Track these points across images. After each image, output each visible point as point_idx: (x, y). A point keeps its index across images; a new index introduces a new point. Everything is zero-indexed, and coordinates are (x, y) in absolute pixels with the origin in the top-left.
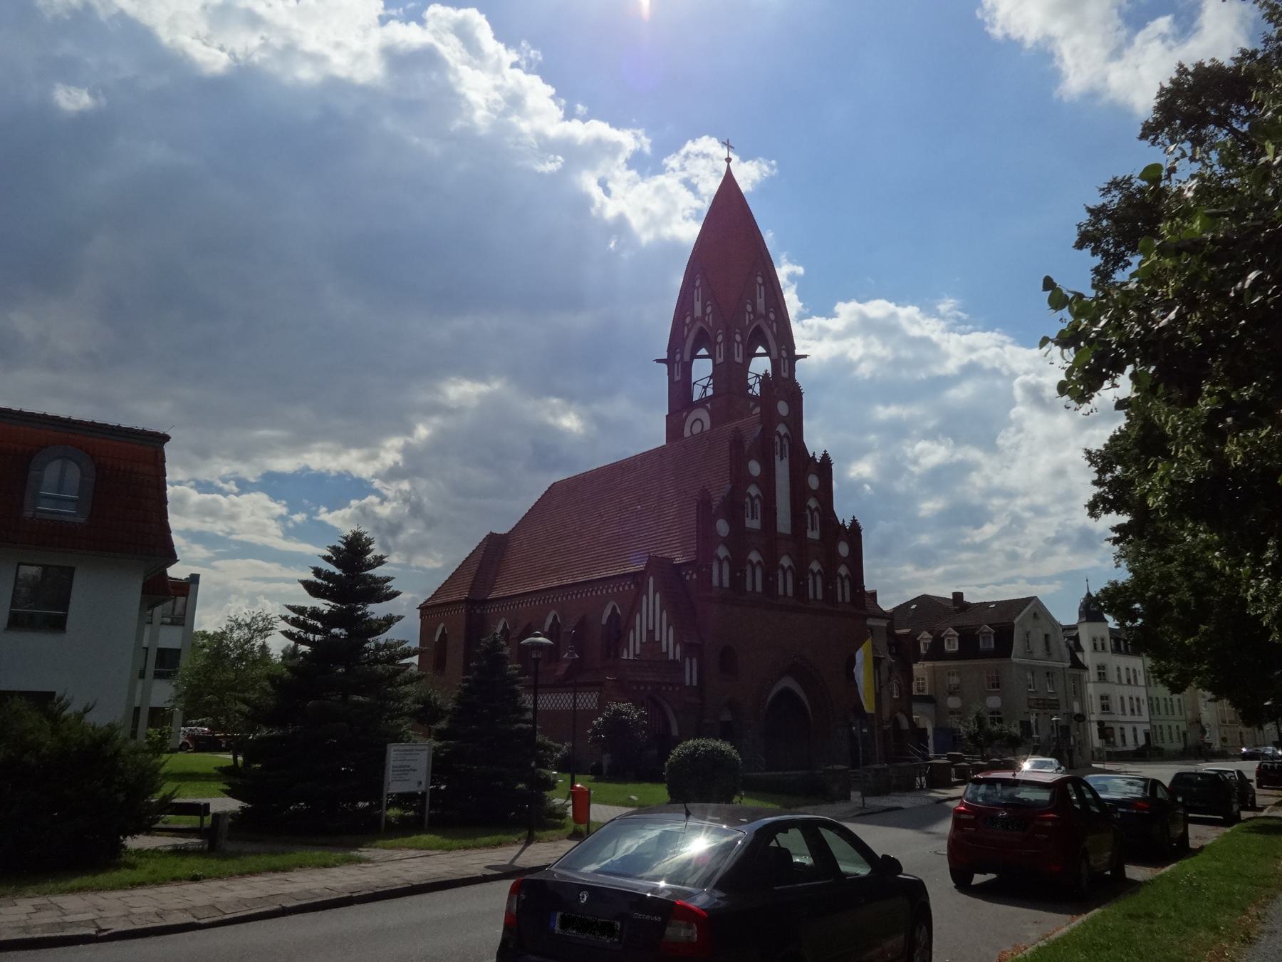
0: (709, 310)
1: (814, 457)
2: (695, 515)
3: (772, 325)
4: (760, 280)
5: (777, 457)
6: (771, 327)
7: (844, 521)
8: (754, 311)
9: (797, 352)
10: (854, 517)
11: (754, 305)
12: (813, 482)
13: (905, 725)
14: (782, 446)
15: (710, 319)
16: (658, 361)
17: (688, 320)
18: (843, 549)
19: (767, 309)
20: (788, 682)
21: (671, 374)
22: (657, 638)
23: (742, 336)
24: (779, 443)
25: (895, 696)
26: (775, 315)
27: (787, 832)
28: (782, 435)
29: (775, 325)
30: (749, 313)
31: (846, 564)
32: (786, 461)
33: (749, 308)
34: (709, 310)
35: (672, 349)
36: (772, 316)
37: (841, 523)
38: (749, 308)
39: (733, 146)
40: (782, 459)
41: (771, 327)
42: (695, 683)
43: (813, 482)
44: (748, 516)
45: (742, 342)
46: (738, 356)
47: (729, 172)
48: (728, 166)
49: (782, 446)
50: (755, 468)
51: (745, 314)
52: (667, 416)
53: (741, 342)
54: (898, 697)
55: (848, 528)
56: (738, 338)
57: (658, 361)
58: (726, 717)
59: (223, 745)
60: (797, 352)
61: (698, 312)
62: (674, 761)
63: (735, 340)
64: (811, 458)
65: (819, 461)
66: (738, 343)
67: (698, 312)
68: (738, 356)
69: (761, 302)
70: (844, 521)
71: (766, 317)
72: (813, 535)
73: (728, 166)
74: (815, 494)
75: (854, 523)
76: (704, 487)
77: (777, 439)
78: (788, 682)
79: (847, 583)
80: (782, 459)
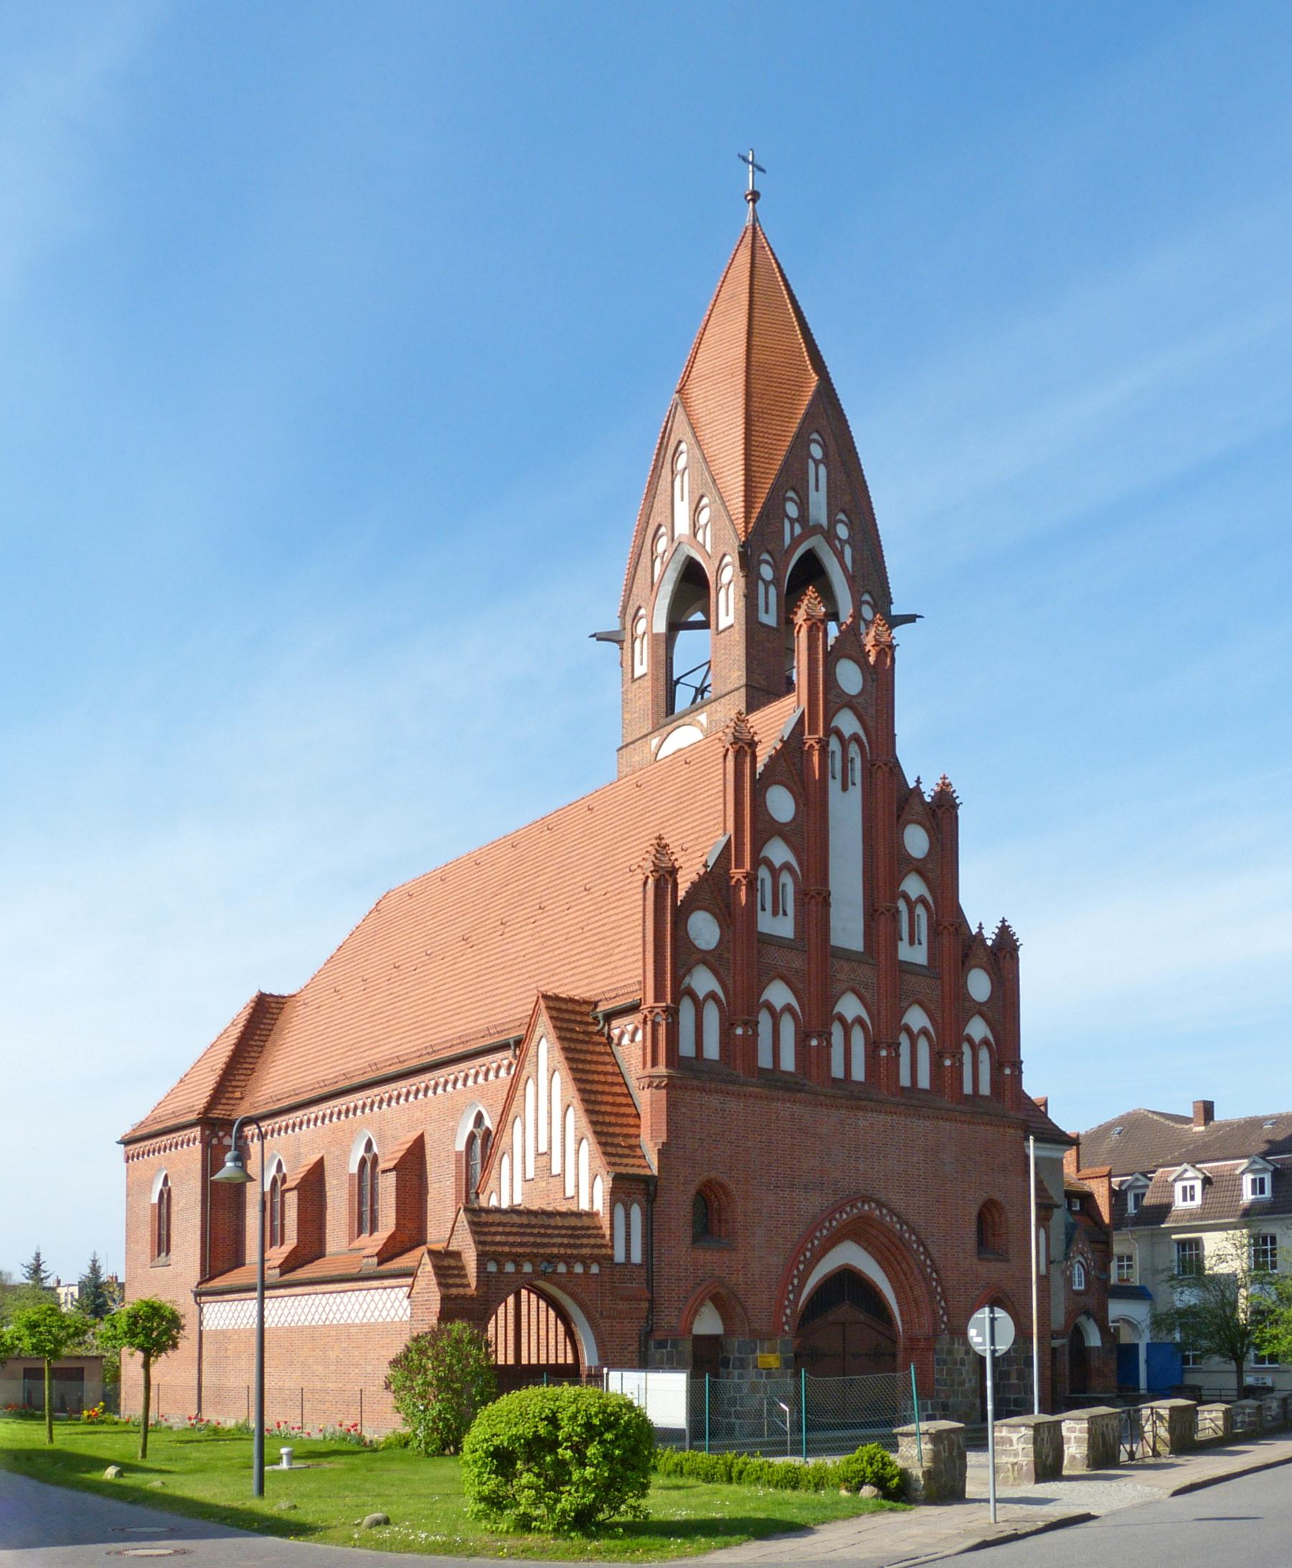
1: (980, 933)
3: (842, 552)
5: (834, 786)
7: (980, 927)
8: (803, 518)
10: (1003, 921)
11: (803, 505)
12: (916, 841)
13: (1094, 1339)
14: (846, 760)
15: (706, 537)
18: (979, 985)
19: (831, 515)
20: (851, 1255)
22: (556, 1169)
23: (775, 568)
24: (838, 756)
25: (1076, 1287)
26: (850, 526)
27: (692, 883)
28: (913, 899)
29: (848, 551)
30: (792, 521)
31: (983, 1016)
32: (856, 793)
33: (792, 510)
34: (704, 517)
36: (842, 531)
37: (974, 930)
38: (792, 510)
39: (763, 166)
40: (845, 788)
41: (840, 556)
42: (637, 1257)
43: (916, 841)
44: (763, 909)
45: (776, 581)
46: (767, 612)
49: (846, 760)
51: (783, 523)
53: (772, 582)
54: (1082, 1288)
55: (989, 943)
58: (708, 1323)
62: (588, 1503)
63: (760, 577)
64: (975, 937)
65: (928, 800)
66: (767, 584)
68: (767, 612)
70: (980, 927)
71: (830, 536)
72: (914, 953)
74: (920, 868)
75: (1004, 932)
77: (902, 905)
78: (851, 1255)
79: (984, 1055)
80: (845, 788)
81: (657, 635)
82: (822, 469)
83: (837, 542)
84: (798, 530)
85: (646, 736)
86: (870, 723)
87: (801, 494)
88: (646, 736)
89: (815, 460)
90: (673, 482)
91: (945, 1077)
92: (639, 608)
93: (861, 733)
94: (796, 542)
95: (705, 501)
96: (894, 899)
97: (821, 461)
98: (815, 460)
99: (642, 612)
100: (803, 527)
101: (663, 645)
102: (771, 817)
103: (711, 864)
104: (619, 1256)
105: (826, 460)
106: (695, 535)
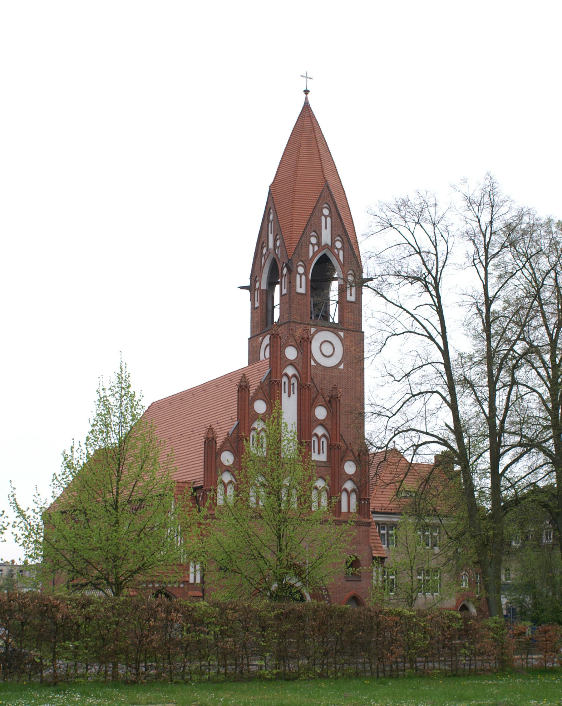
0: (278, 243)
2: (203, 452)
4: (326, 212)
6: (337, 257)
8: (319, 243)
9: (364, 276)
11: (319, 238)
16: (242, 288)
17: (264, 251)
21: (252, 300)
23: (305, 267)
26: (342, 242)
29: (341, 253)
32: (294, 397)
33: (314, 240)
34: (278, 243)
35: (254, 277)
38: (314, 240)
40: (289, 396)
45: (306, 273)
47: (307, 108)
48: (306, 98)
50: (260, 407)
52: (249, 339)
53: (303, 274)
56: (301, 270)
57: (242, 288)
59: (390, 532)
60: (364, 276)
61: (271, 245)
67: (271, 245)
69: (326, 237)
71: (332, 247)
73: (306, 98)
76: (211, 426)
81: (263, 290)
82: (329, 219)
83: (336, 251)
84: (316, 248)
85: (257, 335)
86: (300, 369)
87: (318, 233)
88: (257, 335)
89: (325, 216)
90: (268, 225)
91: (336, 509)
92: (256, 277)
93: (297, 374)
94: (315, 254)
95: (278, 237)
96: (310, 438)
97: (328, 216)
98: (325, 216)
99: (257, 279)
100: (319, 247)
101: (265, 295)
102: (256, 412)
103: (230, 433)
104: (191, 581)
105: (330, 215)
106: (275, 250)
